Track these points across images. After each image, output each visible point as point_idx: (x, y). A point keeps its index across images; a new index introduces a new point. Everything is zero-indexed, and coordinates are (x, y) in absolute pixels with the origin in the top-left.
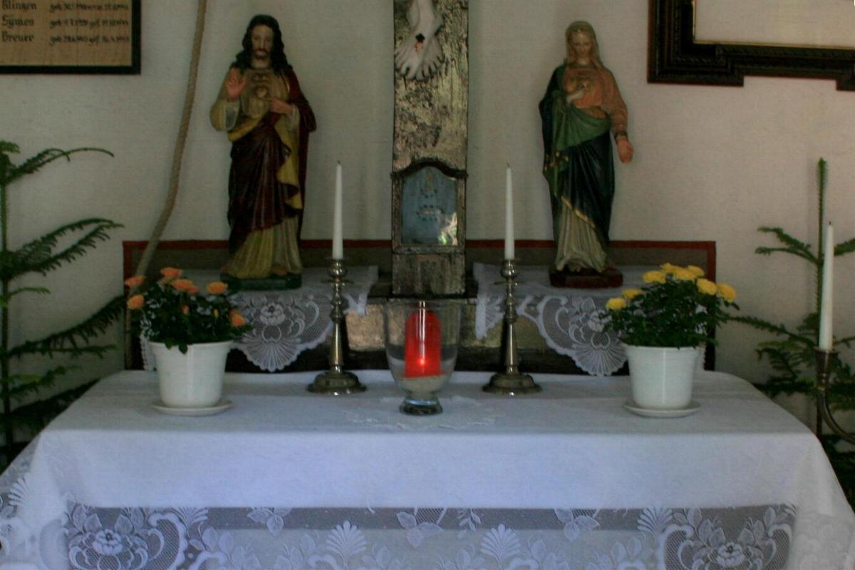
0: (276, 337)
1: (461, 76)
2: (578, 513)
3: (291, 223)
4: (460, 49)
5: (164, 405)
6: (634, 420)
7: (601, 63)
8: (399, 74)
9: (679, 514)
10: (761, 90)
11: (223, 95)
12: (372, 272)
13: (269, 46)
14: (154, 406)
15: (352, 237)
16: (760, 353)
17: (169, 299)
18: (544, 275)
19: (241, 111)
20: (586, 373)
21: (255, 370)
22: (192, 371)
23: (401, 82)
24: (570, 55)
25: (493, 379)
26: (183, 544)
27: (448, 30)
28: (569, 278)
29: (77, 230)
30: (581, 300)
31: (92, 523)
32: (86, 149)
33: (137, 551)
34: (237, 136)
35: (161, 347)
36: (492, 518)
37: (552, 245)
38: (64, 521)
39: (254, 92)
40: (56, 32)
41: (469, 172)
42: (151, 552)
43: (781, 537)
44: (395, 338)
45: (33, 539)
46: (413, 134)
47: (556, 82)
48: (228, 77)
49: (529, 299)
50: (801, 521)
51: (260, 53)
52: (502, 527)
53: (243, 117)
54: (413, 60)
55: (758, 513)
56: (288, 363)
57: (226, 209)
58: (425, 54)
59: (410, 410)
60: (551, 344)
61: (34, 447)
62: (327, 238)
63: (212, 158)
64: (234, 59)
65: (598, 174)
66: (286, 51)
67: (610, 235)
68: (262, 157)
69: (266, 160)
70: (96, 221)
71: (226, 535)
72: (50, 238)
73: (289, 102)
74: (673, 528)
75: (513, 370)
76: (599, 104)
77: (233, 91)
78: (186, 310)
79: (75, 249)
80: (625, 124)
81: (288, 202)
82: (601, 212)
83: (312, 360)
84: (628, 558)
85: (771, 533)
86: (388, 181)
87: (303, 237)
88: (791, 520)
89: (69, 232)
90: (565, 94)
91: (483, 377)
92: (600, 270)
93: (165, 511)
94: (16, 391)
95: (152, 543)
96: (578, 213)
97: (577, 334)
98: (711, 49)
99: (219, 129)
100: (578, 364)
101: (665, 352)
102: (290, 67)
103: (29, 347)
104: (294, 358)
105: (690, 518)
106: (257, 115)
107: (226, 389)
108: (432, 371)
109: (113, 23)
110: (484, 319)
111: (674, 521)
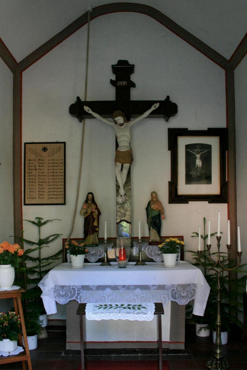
0: (93, 256)
1: (130, 203)
2: (153, 286)
3: (96, 234)
4: (129, 198)
5: (72, 266)
6: (164, 268)
7: (158, 200)
8: (117, 203)
9: (173, 286)
10: (192, 204)
11: (83, 208)
12: (113, 244)
13: (91, 198)
14: (71, 267)
15: (109, 237)
16: (193, 259)
17: (72, 247)
18: (148, 243)
19: (86, 211)
20: (156, 262)
21: (90, 262)
22: (77, 260)
23: (118, 205)
24: (152, 198)
25: (137, 263)
26: (77, 292)
27: (127, 194)
28: (152, 243)
29: (53, 236)
30: (155, 248)
31: (59, 288)
32: (56, 219)
33: (68, 294)
34: (85, 216)
35: (72, 256)
36: (136, 287)
37: (149, 238)
38: (54, 288)
39: (89, 207)
40: (49, 197)
41: (132, 222)
42: (71, 294)
43: (194, 290)
44: (118, 255)
45: (48, 291)
46: (120, 215)
47: (149, 204)
48: (84, 205)
49: (144, 247)
50: (198, 286)
51: (90, 200)
52: (138, 289)
53: (86, 213)
54: (120, 200)
55: (189, 285)
56: (96, 261)
57: (83, 231)
58: (122, 199)
59: (120, 267)
60: (149, 256)
61: (48, 274)
62: (103, 237)
63: (80, 221)
64: (85, 201)
65: (158, 222)
66: (95, 199)
67: (161, 235)
68: (90, 221)
69: (91, 221)
70: (57, 234)
71: (85, 291)
72: (48, 238)
73: (96, 209)
74: (172, 288)
75: (142, 262)
76: (158, 208)
77: (85, 207)
78: (77, 249)
79: (54, 239)
80: (163, 212)
81: (96, 229)
82: (159, 230)
83: (100, 260)
84: (163, 294)
85: (192, 289)
86: (115, 225)
87: (99, 237)
88: (196, 287)
89: (52, 236)
90: (151, 206)
91: (135, 263)
92: (159, 242)
93: (73, 286)
94: (43, 267)
95: (71, 292)
96: (154, 230)
97: (154, 254)
98: (181, 196)
99: (82, 215)
100: (154, 260)
101: (170, 255)
102: (96, 202)
103: (44, 259)
104: (97, 260)
105: (175, 286)
106: (89, 212)
107: (84, 266)
108: (124, 260)
109: (60, 195)
110: (135, 251)
111: (172, 287)
